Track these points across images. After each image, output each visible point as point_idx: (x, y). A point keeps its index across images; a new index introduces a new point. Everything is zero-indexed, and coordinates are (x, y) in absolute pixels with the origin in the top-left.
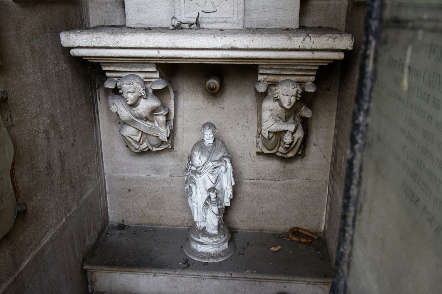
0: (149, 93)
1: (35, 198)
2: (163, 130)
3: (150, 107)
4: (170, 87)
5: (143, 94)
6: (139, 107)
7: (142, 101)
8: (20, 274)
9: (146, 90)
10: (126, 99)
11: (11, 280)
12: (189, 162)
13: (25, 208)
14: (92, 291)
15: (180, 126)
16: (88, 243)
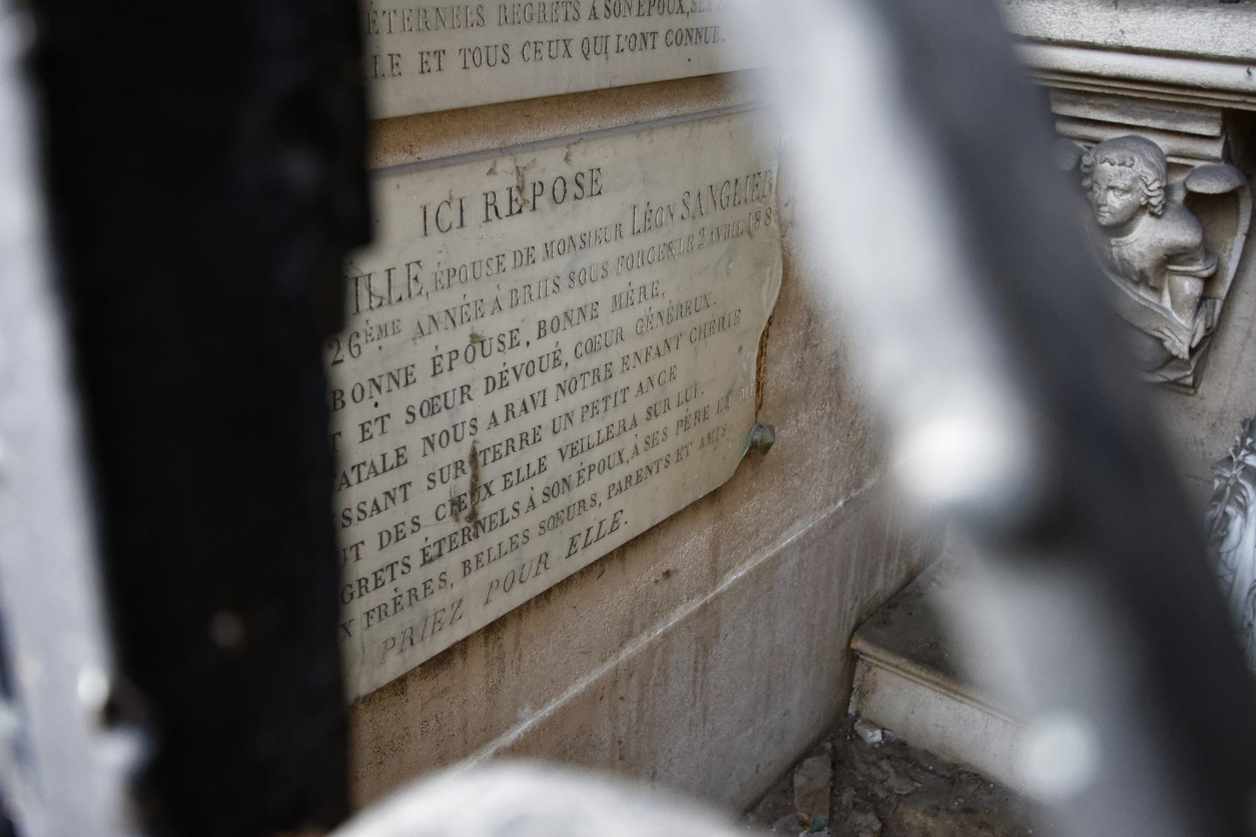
0: (1173, 202)
1: (793, 423)
2: (1183, 322)
3: (1164, 243)
4: (1248, 193)
5: (1153, 201)
6: (1130, 238)
7: (1145, 221)
8: (718, 598)
9: (1167, 190)
10: (1100, 206)
11: (696, 604)
12: (1243, 440)
13: (770, 440)
14: (858, 714)
15: (1242, 323)
16: (879, 584)
